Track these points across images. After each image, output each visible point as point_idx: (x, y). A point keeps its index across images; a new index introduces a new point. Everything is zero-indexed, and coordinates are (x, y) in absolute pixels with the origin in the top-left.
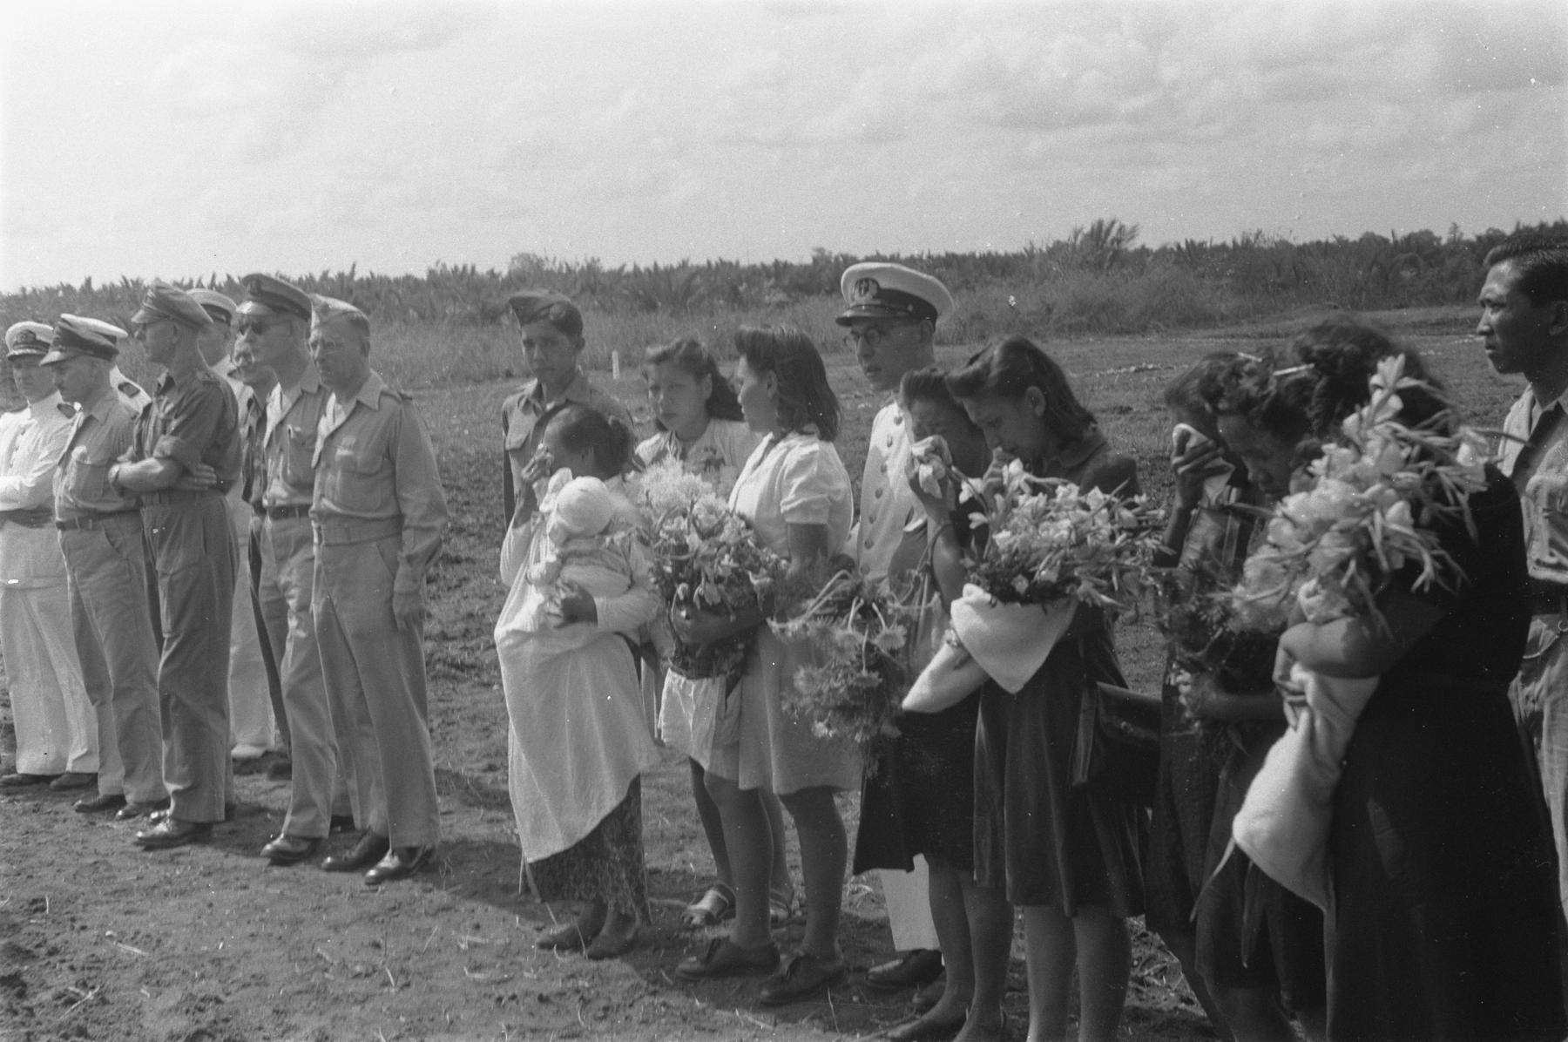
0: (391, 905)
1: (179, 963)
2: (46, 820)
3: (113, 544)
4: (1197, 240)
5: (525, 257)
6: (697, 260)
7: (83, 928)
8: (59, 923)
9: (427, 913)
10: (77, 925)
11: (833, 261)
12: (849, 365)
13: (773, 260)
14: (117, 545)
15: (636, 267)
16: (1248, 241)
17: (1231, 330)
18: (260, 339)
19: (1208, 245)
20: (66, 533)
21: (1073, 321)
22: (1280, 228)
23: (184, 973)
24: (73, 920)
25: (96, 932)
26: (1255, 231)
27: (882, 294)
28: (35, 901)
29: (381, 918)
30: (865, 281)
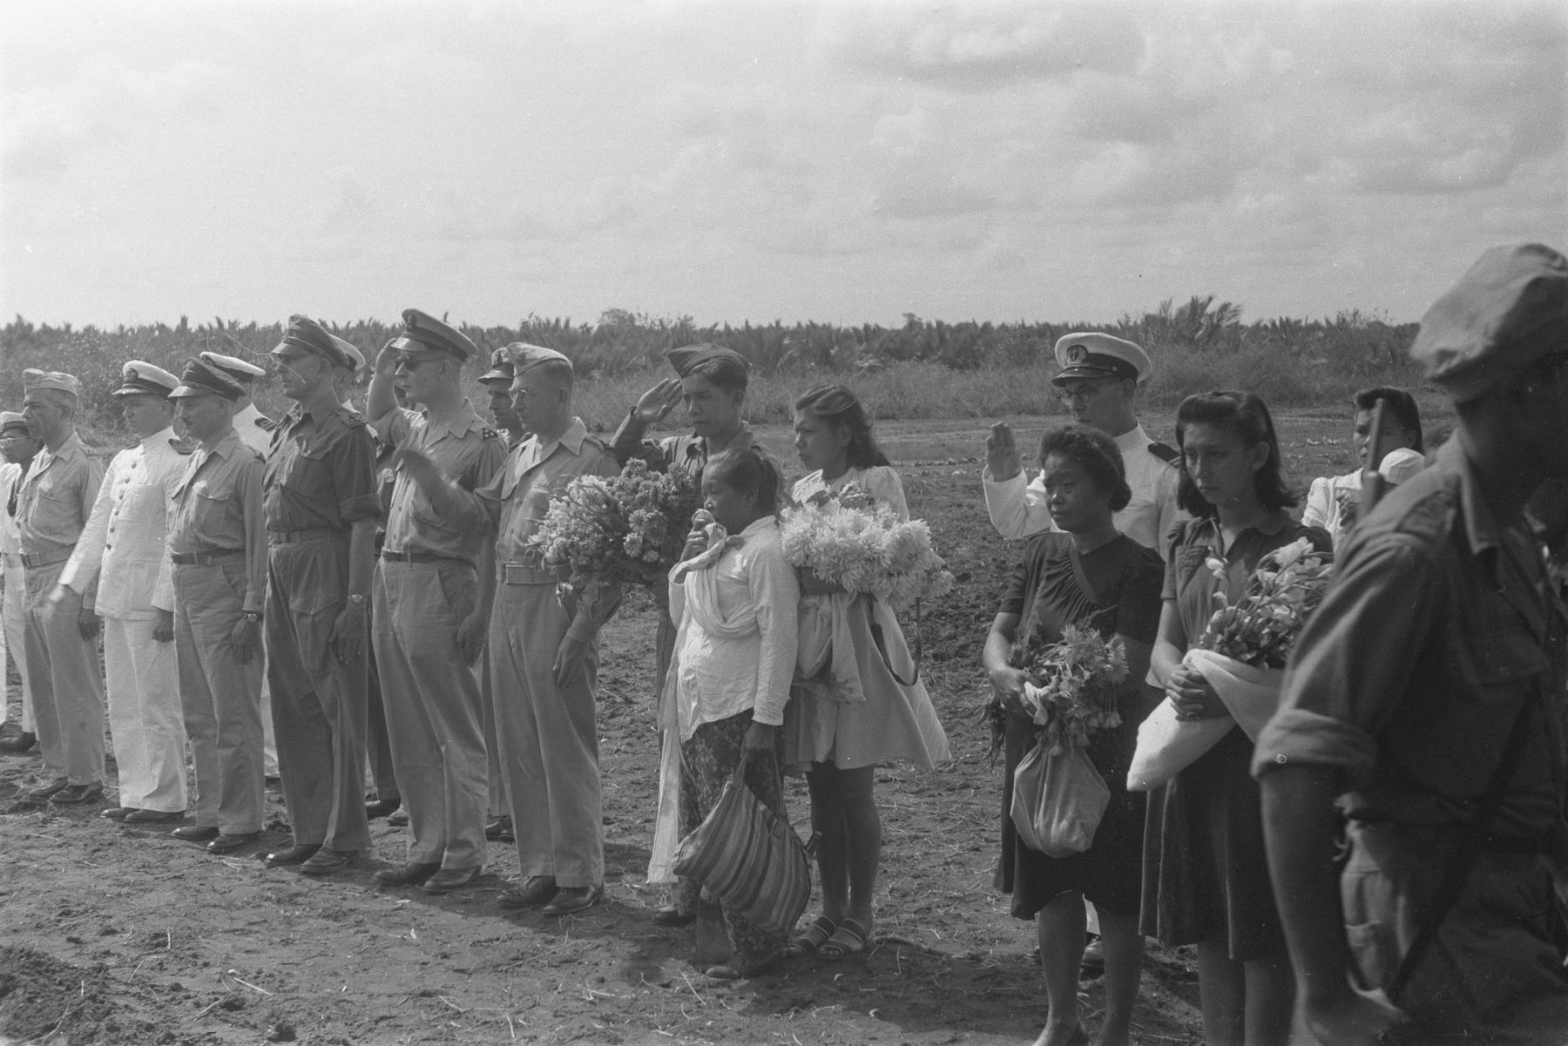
0: (512, 955)
1: (304, 1005)
2: (161, 855)
3: (229, 582)
4: (1293, 318)
5: (612, 312)
6: (789, 322)
7: (206, 965)
8: (181, 959)
9: (551, 966)
10: (200, 962)
11: (925, 326)
12: (942, 431)
13: (275, 322)
14: (233, 582)
15: (727, 327)
16: (1344, 320)
17: (1329, 409)
18: (412, 374)
19: (1303, 323)
20: (182, 567)
21: (1167, 395)
22: (1376, 310)
23: (310, 1014)
24: (195, 956)
25: (219, 970)
26: (1351, 311)
27: (1090, 357)
28: (157, 936)
29: (504, 969)
30: (1075, 349)
